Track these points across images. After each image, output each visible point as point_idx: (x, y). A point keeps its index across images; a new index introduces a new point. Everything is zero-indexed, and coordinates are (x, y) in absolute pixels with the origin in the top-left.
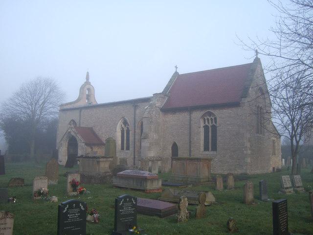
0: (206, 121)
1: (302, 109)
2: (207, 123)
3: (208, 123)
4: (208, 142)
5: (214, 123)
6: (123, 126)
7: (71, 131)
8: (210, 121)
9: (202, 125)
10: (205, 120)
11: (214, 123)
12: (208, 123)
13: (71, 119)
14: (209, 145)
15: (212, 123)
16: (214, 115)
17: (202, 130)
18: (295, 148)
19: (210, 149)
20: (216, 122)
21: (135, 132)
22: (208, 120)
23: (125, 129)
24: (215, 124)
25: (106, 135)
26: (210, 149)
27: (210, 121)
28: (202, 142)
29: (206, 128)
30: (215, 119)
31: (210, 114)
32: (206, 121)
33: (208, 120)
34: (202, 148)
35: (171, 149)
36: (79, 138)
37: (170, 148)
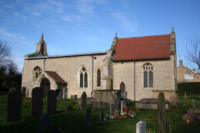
0: (146, 69)
2: (146, 70)
3: (147, 70)
6: (82, 71)
8: (148, 69)
10: (144, 68)
12: (147, 70)
13: (36, 66)
15: (149, 70)
17: (143, 74)
20: (152, 70)
22: (147, 68)
23: (84, 73)
24: (146, 71)
27: (148, 69)
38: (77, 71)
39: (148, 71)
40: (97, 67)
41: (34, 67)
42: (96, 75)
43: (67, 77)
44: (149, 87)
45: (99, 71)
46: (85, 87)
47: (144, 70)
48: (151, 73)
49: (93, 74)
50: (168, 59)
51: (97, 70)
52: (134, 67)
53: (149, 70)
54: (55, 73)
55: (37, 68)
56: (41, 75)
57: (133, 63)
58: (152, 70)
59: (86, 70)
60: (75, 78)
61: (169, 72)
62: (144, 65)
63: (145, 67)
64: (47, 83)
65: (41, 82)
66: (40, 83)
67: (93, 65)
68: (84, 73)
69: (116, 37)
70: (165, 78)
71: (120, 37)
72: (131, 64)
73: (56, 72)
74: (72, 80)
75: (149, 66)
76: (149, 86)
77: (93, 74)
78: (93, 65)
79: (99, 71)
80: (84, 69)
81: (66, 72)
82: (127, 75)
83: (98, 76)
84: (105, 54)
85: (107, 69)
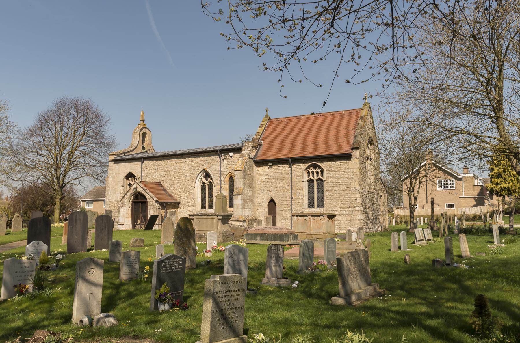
0: (311, 174)
1: (409, 135)
2: (311, 177)
3: (313, 176)
4: (313, 198)
5: (320, 176)
6: (204, 180)
7: (138, 186)
8: (315, 174)
9: (306, 178)
10: (308, 173)
11: (320, 176)
12: (313, 176)
13: (128, 172)
14: (205, 201)
15: (318, 176)
16: (320, 167)
17: (306, 184)
18: (112, 285)
19: (92, 223)
20: (322, 175)
21: (221, 187)
22: (313, 173)
23: (207, 184)
24: (321, 178)
25: (180, 192)
26: (92, 223)
27: (315, 174)
28: (199, 200)
29: (310, 181)
30: (322, 172)
31: (315, 166)
32: (311, 174)
33: (313, 173)
34: (306, 205)
35: (267, 206)
36: (148, 195)
37: (266, 205)
38: (196, 175)
39: (315, 178)
40: (228, 172)
41: (126, 174)
42: (227, 186)
43: (180, 192)
44: (317, 208)
45: (231, 179)
46: (209, 208)
47: (309, 176)
48: (320, 181)
49: (221, 184)
50: (347, 157)
51: (227, 178)
52: (290, 171)
53: (318, 176)
54: (159, 184)
55: (130, 175)
56: (132, 188)
57: (287, 167)
58: (322, 175)
59: (211, 179)
60: (192, 193)
61: (350, 180)
62: (308, 168)
63: (310, 171)
64: (142, 202)
65: (133, 202)
66: (131, 202)
67: (221, 169)
68: (207, 184)
69: (266, 116)
70: (344, 190)
71: (273, 116)
72: (285, 168)
73: (162, 183)
74: (188, 197)
75: (317, 169)
76: (318, 205)
77: (221, 184)
78: (221, 169)
79: (231, 179)
80: (207, 175)
81: (177, 181)
82: (280, 185)
83: (229, 188)
84: (237, 150)
85: (242, 176)
